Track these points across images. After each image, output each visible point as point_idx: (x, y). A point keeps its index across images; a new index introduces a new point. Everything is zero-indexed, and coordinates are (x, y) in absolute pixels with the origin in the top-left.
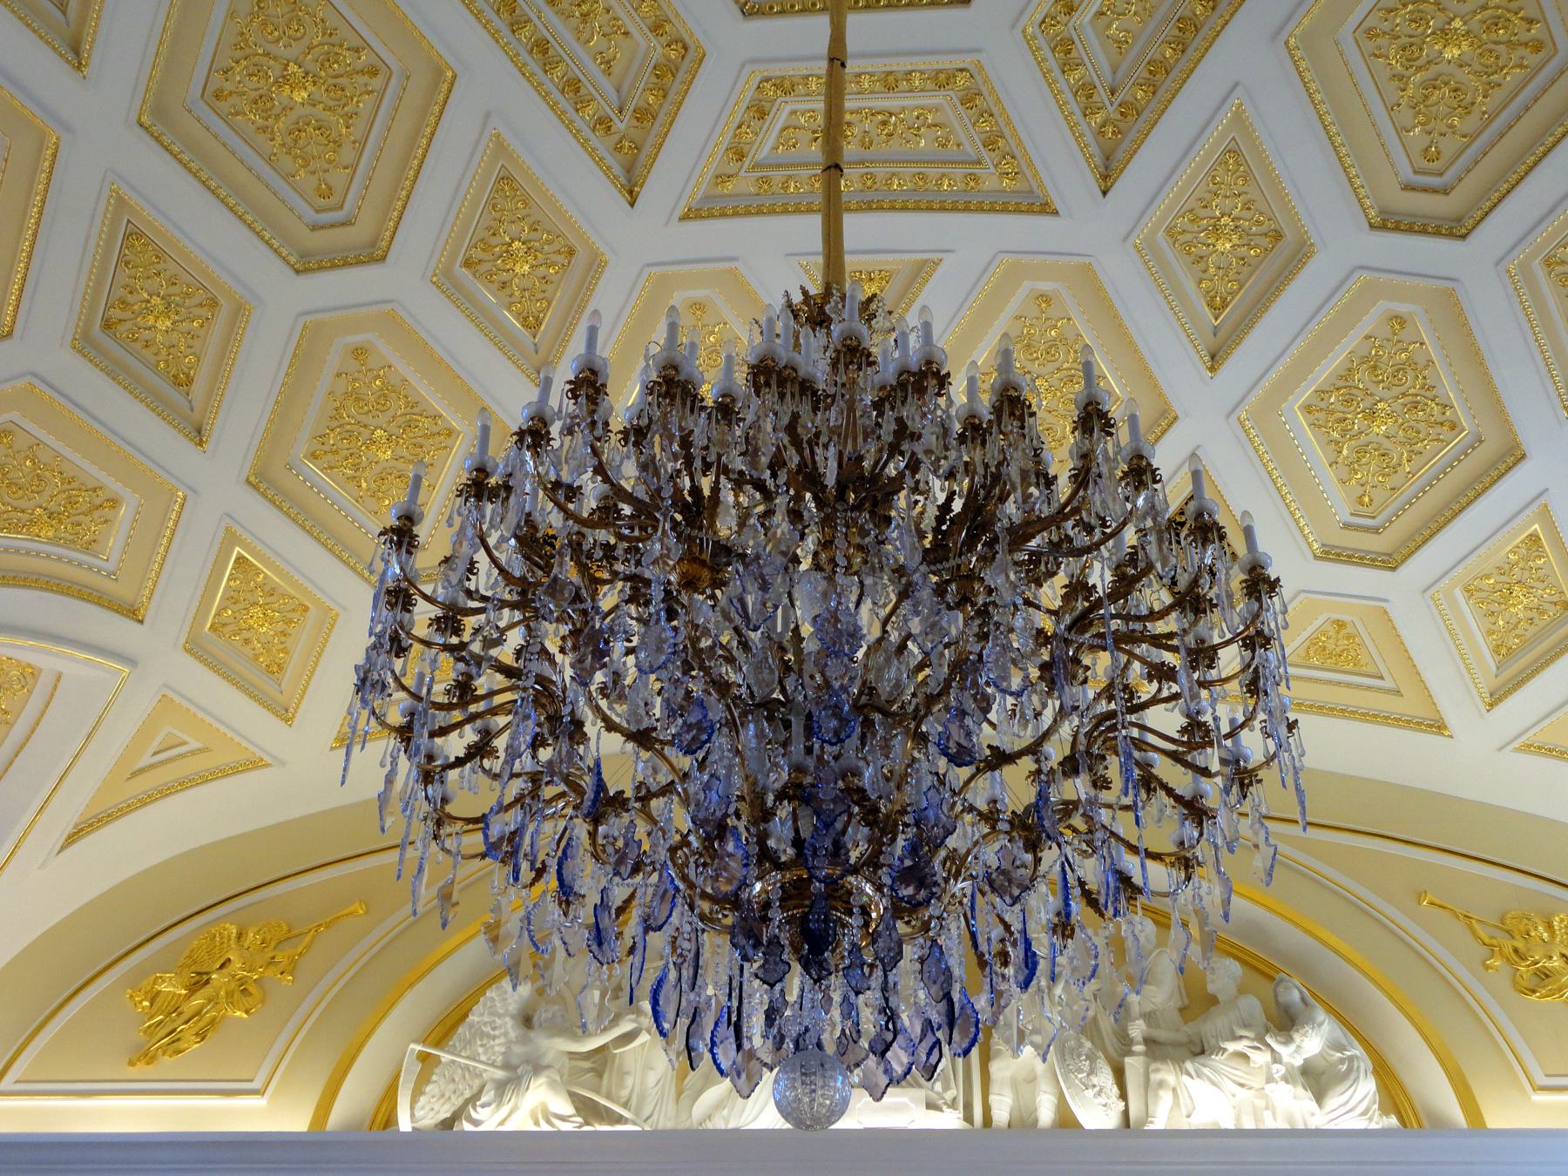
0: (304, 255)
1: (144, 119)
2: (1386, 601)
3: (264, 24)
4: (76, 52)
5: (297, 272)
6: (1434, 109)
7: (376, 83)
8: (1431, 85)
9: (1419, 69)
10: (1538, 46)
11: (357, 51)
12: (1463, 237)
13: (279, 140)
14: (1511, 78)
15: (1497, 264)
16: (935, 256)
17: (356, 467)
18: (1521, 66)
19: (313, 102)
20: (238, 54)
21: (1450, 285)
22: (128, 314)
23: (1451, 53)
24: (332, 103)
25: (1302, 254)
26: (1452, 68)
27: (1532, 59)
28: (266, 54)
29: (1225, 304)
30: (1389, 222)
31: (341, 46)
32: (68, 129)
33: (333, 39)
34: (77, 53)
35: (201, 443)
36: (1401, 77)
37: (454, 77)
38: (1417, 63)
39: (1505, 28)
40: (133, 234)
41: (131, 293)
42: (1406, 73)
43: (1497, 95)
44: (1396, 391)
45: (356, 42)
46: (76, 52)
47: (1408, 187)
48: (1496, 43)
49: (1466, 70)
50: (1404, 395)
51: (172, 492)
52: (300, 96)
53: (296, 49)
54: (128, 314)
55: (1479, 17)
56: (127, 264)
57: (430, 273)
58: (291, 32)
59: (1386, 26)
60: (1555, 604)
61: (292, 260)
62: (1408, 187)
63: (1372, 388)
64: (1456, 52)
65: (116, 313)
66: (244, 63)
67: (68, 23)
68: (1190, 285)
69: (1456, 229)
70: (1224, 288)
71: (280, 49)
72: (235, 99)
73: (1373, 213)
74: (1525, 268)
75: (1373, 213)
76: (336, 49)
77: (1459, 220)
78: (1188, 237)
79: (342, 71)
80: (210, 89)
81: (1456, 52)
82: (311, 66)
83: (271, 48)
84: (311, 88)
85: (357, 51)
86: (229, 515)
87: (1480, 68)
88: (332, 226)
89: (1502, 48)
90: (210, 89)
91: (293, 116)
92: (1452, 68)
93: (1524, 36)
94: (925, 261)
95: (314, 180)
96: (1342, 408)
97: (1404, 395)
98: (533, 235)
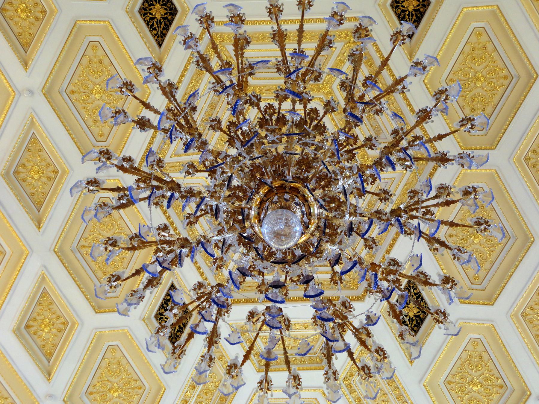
1: (66, 399)
3: (109, 371)
7: (140, 391)
9: (466, 394)
10: (501, 387)
11: (136, 381)
19: (119, 397)
20: (91, 233)
24: (125, 398)
27: (501, 391)
28: (108, 380)
34: (49, 375)
37: (165, 389)
41: (38, 315)
43: (494, 255)
44: (479, 373)
45: (136, 378)
52: (116, 394)
53: (117, 380)
65: (31, 323)
67: (49, 366)
71: (112, 379)
76: (130, 380)
79: (130, 387)
82: (121, 385)
83: (102, 232)
84: (120, 392)
85: (136, 381)
87: (485, 394)
88: (111, 298)
96: (461, 382)
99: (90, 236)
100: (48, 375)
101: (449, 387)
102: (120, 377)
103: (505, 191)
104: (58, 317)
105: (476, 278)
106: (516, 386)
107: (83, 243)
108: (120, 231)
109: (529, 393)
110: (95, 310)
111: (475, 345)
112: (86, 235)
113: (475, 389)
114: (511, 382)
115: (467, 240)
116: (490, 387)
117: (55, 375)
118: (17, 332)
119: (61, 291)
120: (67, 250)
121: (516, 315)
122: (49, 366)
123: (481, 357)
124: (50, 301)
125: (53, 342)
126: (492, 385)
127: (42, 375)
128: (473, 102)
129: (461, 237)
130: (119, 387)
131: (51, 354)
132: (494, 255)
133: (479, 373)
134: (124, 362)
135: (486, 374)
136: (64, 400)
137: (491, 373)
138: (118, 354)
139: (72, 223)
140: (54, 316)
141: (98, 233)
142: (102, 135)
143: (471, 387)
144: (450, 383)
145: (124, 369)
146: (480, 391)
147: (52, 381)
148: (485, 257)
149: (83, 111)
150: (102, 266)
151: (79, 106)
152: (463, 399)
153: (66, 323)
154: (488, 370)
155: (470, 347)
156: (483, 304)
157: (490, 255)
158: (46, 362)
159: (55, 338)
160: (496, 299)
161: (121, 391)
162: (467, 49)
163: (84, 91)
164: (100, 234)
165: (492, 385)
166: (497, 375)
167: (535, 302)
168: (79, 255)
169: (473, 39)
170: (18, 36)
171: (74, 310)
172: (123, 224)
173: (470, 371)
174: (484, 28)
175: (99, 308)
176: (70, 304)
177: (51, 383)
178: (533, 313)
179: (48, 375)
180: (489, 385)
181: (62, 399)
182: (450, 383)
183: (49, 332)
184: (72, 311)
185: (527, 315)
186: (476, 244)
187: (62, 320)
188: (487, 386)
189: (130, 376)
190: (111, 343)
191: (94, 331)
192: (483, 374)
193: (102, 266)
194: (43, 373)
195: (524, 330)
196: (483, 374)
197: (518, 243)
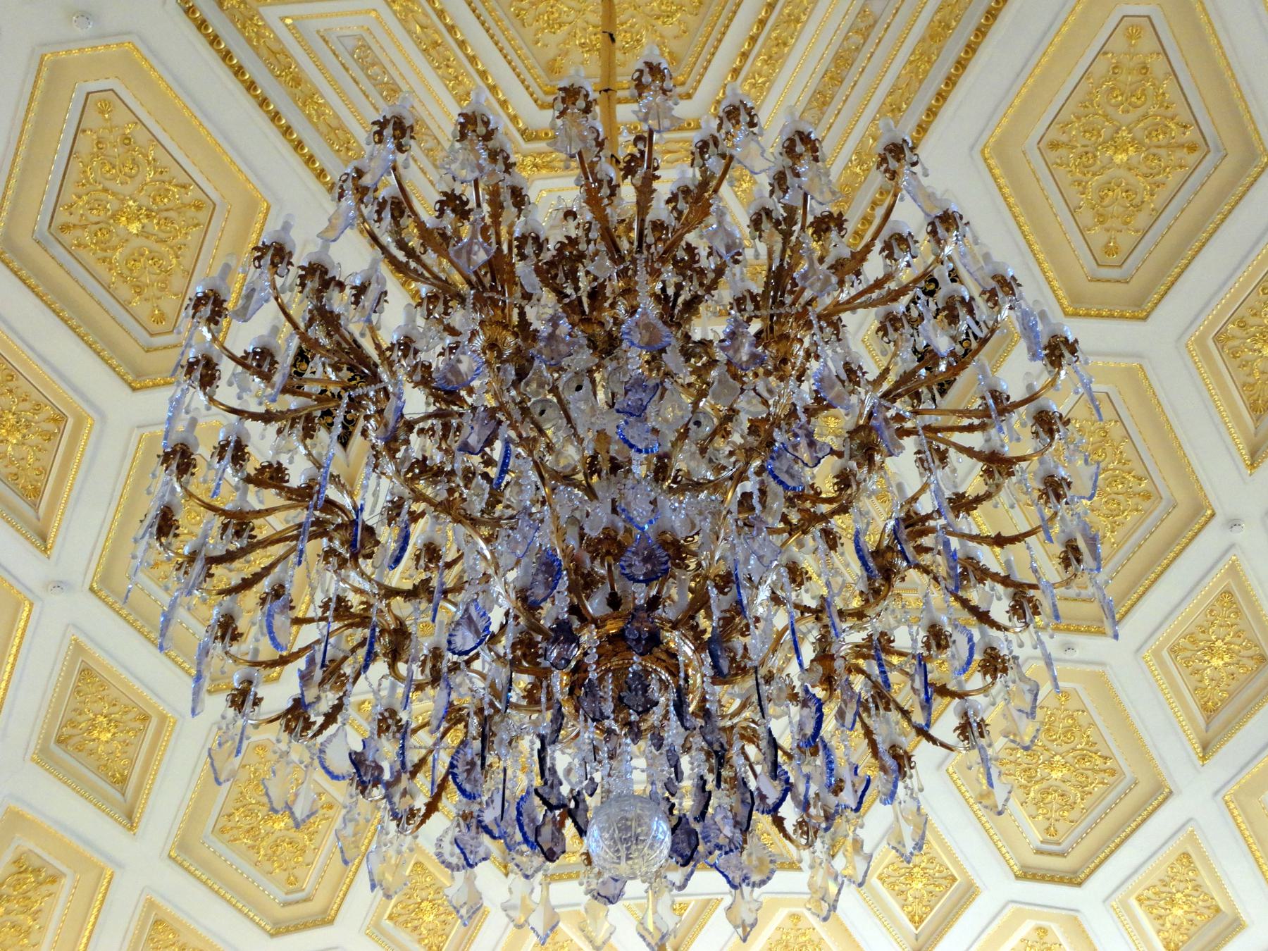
0: (276, 923)
2: (1102, 664)
3: (103, 164)
4: (130, 819)
5: (134, 389)
6: (1110, 209)
7: (203, 216)
8: (1046, 792)
9: (1036, 782)
10: (1147, 496)
12: (1145, 319)
13: (262, 852)
14: (1130, 518)
15: (1104, 901)
16: (719, 897)
17: (255, 838)
18: (1103, 783)
19: (144, 233)
20: (81, 190)
21: (1098, 669)
22: (75, 731)
23: (1056, 775)
24: (163, 235)
25: (969, 893)
26: (1058, 783)
28: (105, 190)
29: (921, 920)
30: (1028, 874)
31: (170, 183)
32: (120, 866)
33: (166, 177)
34: (44, 538)
35: (131, 828)
36: (1025, 787)
37: (268, 208)
38: (1092, 169)
39: (1165, 133)
40: (86, 672)
42: (1085, 179)
43: (1162, 195)
44: (1066, 747)
45: (183, 179)
46: (130, 819)
47: (1039, 852)
48: (1117, 494)
49: (1097, 513)
50: (1074, 749)
51: (102, 870)
53: (130, 188)
54: (75, 731)
55: (1141, 125)
56: (79, 692)
57: (364, 928)
58: (127, 170)
59: (1012, 758)
60: (1252, 657)
61: (268, 928)
62: (1039, 852)
63: (1048, 744)
64: (1060, 774)
66: (85, 198)
68: (894, 905)
69: (1073, 879)
70: (919, 909)
71: (116, 186)
72: (78, 232)
73: (1016, 868)
74: (1124, 904)
75: (1016, 868)
76: (167, 186)
77: (1075, 872)
78: (892, 879)
79: (171, 205)
80: (218, 827)
81: (1060, 774)
83: (108, 184)
84: (145, 221)
85: (184, 187)
86: (75, 626)
87: (1145, 170)
88: (297, 902)
89: (1089, 773)
90: (218, 827)
91: (272, 838)
92: (1122, 172)
93: (1138, 489)
94: (709, 901)
95: (285, 874)
97: (1074, 749)
98: (437, 896)
99: (80, 197)
100: (42, 538)
101: (1052, 156)
102: (138, 179)
103: (1208, 30)
104: (37, 408)
105: (1108, 251)
106: (1180, 496)
107: (63, 217)
108: (158, 176)
109: (1209, 512)
110: (130, 385)
111: (1133, 35)
112: (69, 196)
113: (1120, 158)
114: (1168, 485)
115: (1095, 156)
116: (1163, 152)
117: (59, 539)
118: (44, 757)
119: (32, 349)
120: (25, 241)
121: (1201, 341)
122: (38, 519)
123: (1144, 68)
124: (7, 372)
125: (37, 464)
126: (1093, 770)
127: (27, 544)
128: (1102, 198)
129: (1080, 150)
130: (140, 208)
131: (38, 492)
132: (1162, 195)
133: (1134, 115)
134: (141, 137)
135: (1155, 115)
136: (91, 589)
137: (1127, 467)
138: (121, 115)
139: (23, 171)
140: (27, 405)
141: (100, 187)
142: (161, 318)
143: (1110, 153)
144: (1054, 145)
145: (145, 156)
146: (1134, 162)
147: (54, 553)
148: (1137, 200)
149: (101, 269)
150: (126, 272)
151: (88, 256)
152: (1085, 188)
153: (59, 419)
154: (1161, 106)
155: (1119, 43)
156: (1122, 317)
157: (1152, 195)
158: (119, 796)
159: (39, 455)
160: (1156, 304)
161: (148, 216)
162: (1102, 67)
163: (97, 219)
164: (105, 190)
165: (1093, 770)
166: (1185, 116)
167: (1252, 308)
168: (59, 251)
169: (1119, 43)
170: (103, 769)
171: (75, 389)
172: (165, 160)
173: (1110, 110)
174: (1149, 17)
175: (139, 375)
176: (61, 376)
177: (54, 558)
178: (1243, 334)
179: (42, 538)
180: (1117, 494)
181: (165, 854)
182: (1054, 145)
183: (21, 444)
184: (71, 393)
185: (1228, 338)
186: (1119, 167)
187: (48, 411)
188: (1154, 150)
189: (166, 177)
190: (93, 86)
191: (136, 433)
192: (1145, 116)
193: (126, 272)
194: (27, 538)
195: (1216, 373)
196: (1145, 116)
197: (1227, 166)
